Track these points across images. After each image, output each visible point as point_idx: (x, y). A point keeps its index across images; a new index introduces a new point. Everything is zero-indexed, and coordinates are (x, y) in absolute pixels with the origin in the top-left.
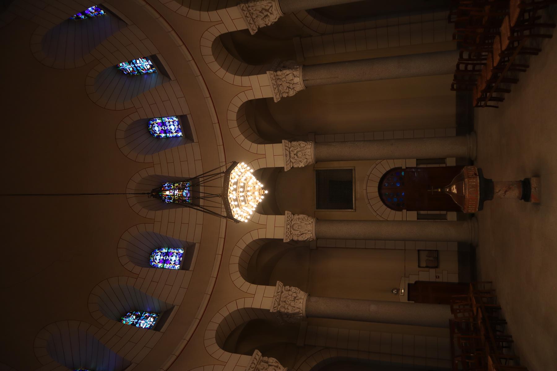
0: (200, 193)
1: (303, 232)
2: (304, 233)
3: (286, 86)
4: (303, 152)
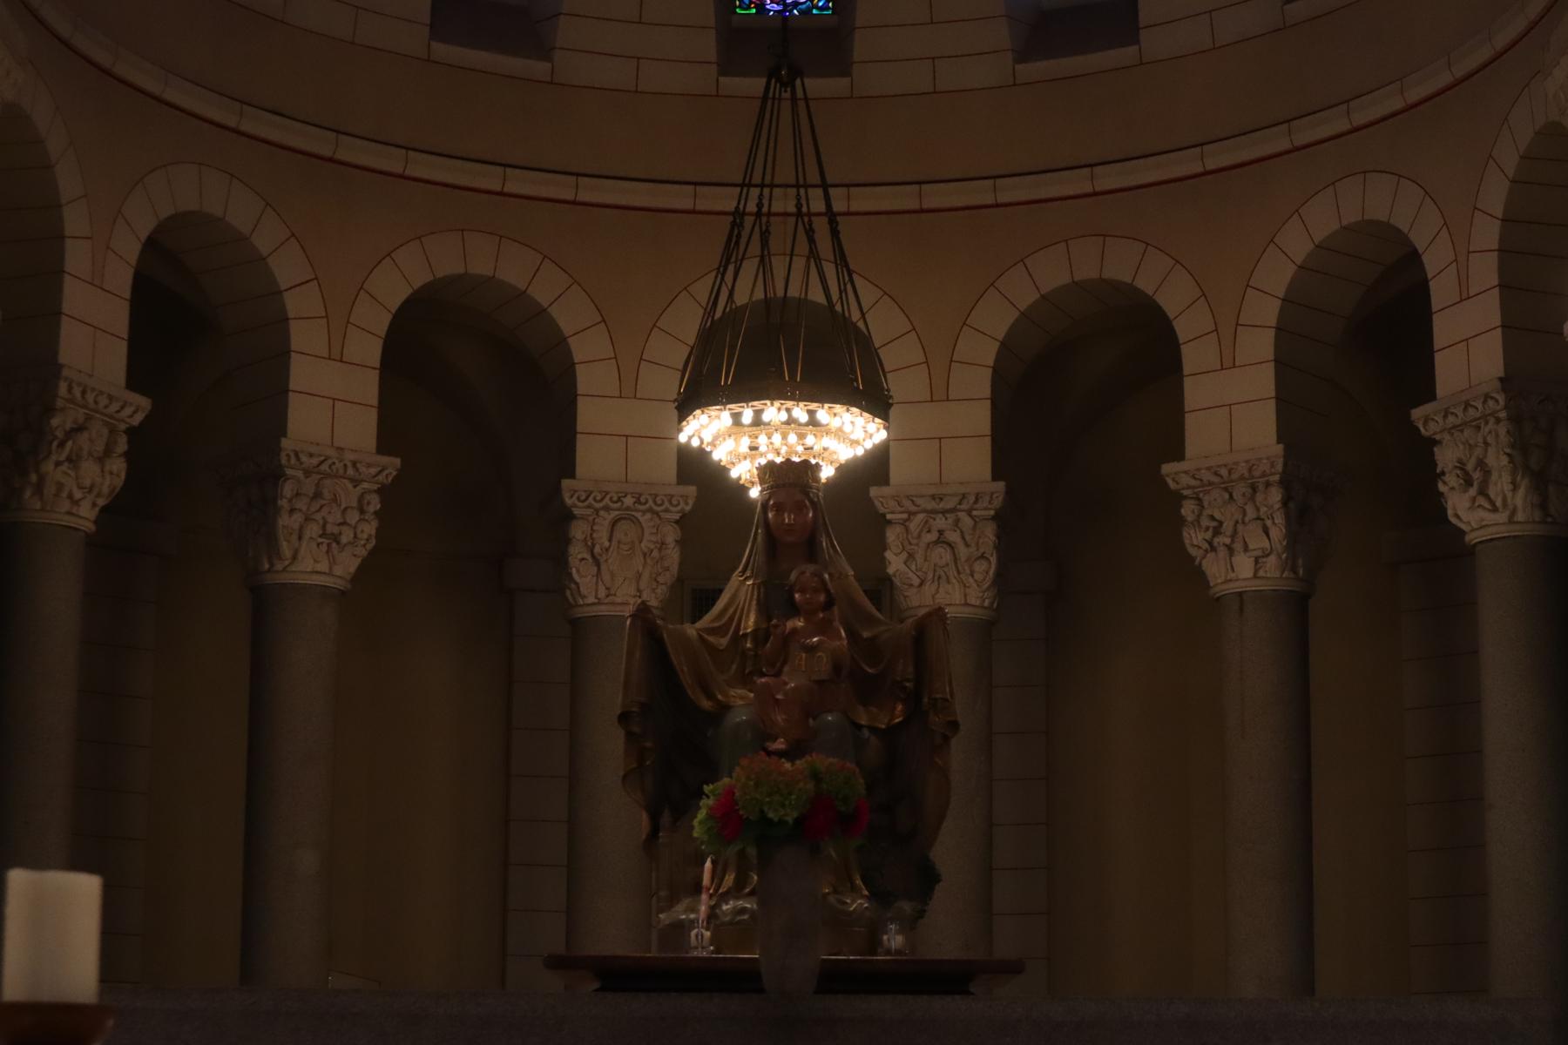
0: (788, 295)
1: (603, 567)
2: (599, 569)
3: (1222, 519)
4: (952, 572)
